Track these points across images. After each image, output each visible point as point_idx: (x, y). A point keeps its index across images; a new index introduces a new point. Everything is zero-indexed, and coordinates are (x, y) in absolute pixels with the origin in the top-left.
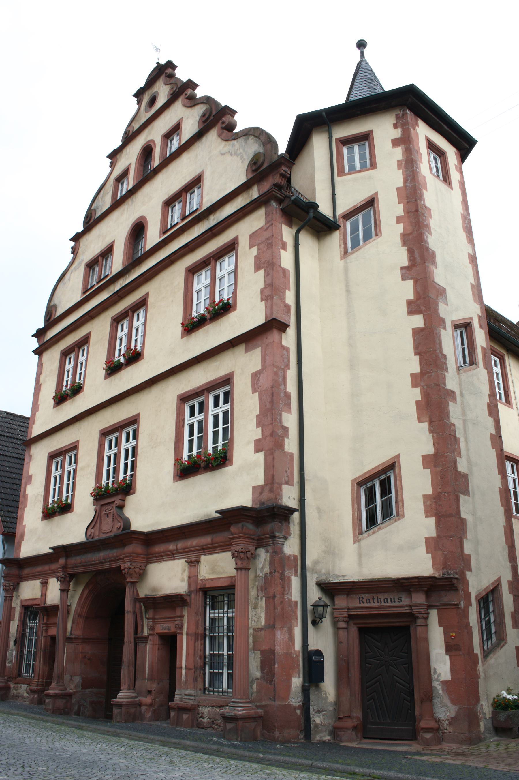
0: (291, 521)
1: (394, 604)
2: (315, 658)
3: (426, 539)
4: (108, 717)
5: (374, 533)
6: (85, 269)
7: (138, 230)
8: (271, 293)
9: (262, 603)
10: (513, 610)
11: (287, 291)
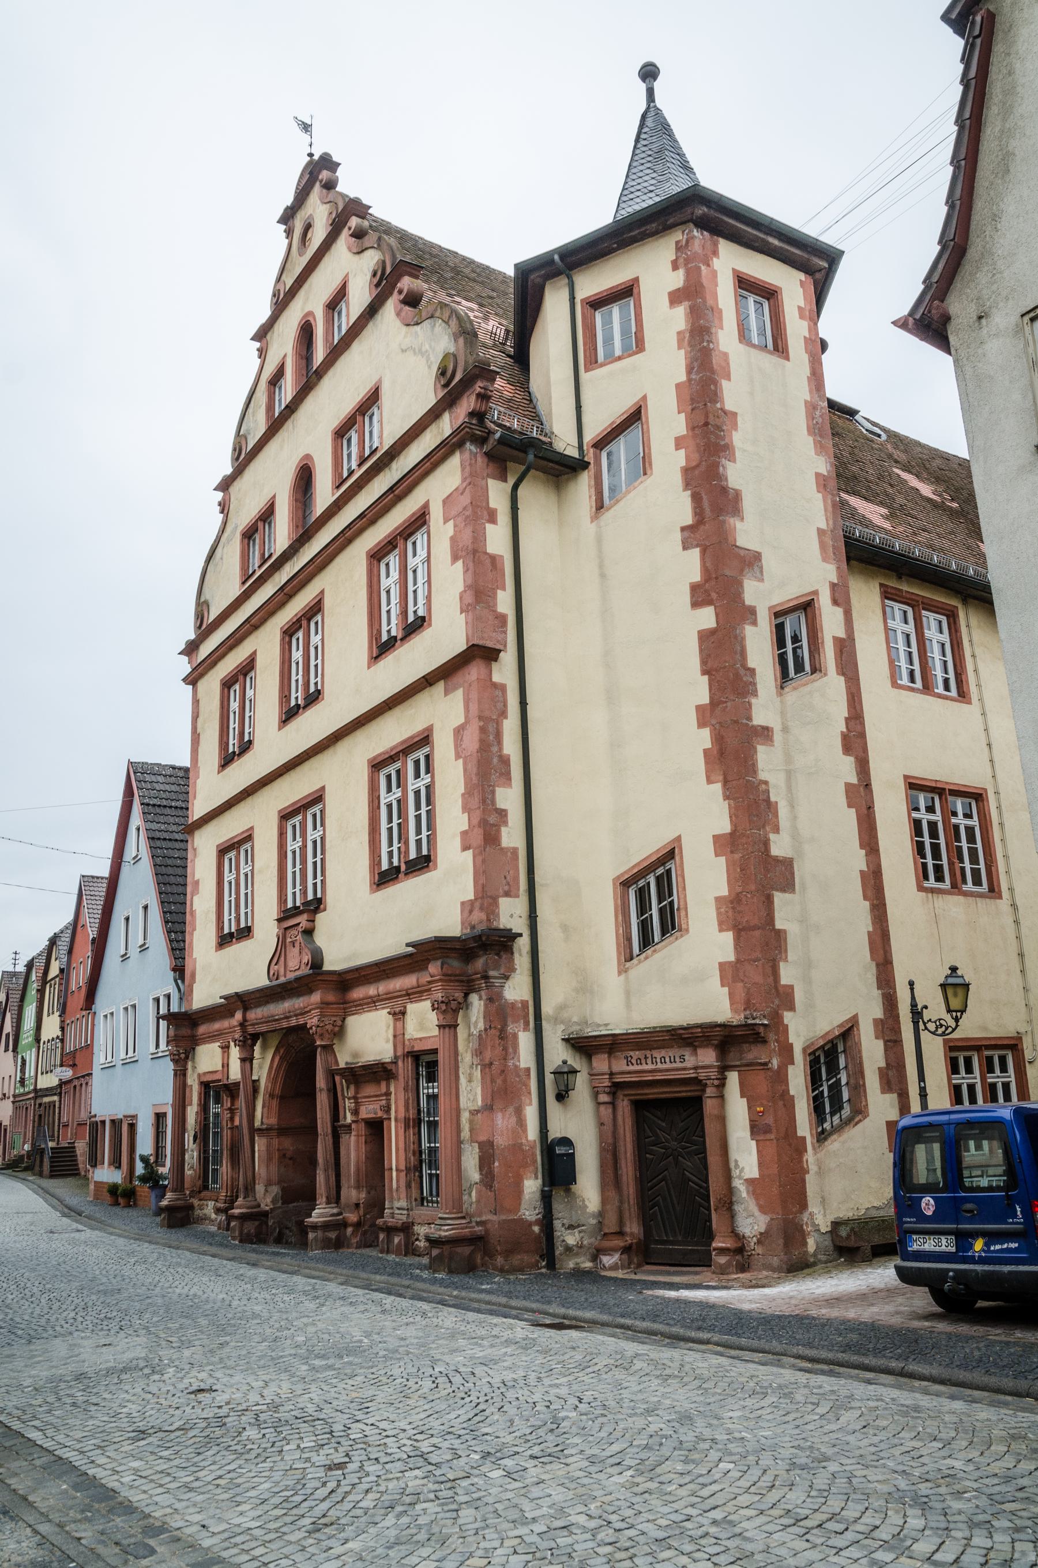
0: (514, 950)
1: (674, 1065)
2: (559, 1150)
3: (721, 964)
4: (303, 1244)
5: (646, 958)
6: (242, 541)
7: (305, 478)
8: (478, 596)
9: (477, 1074)
10: (883, 1064)
11: (499, 592)
